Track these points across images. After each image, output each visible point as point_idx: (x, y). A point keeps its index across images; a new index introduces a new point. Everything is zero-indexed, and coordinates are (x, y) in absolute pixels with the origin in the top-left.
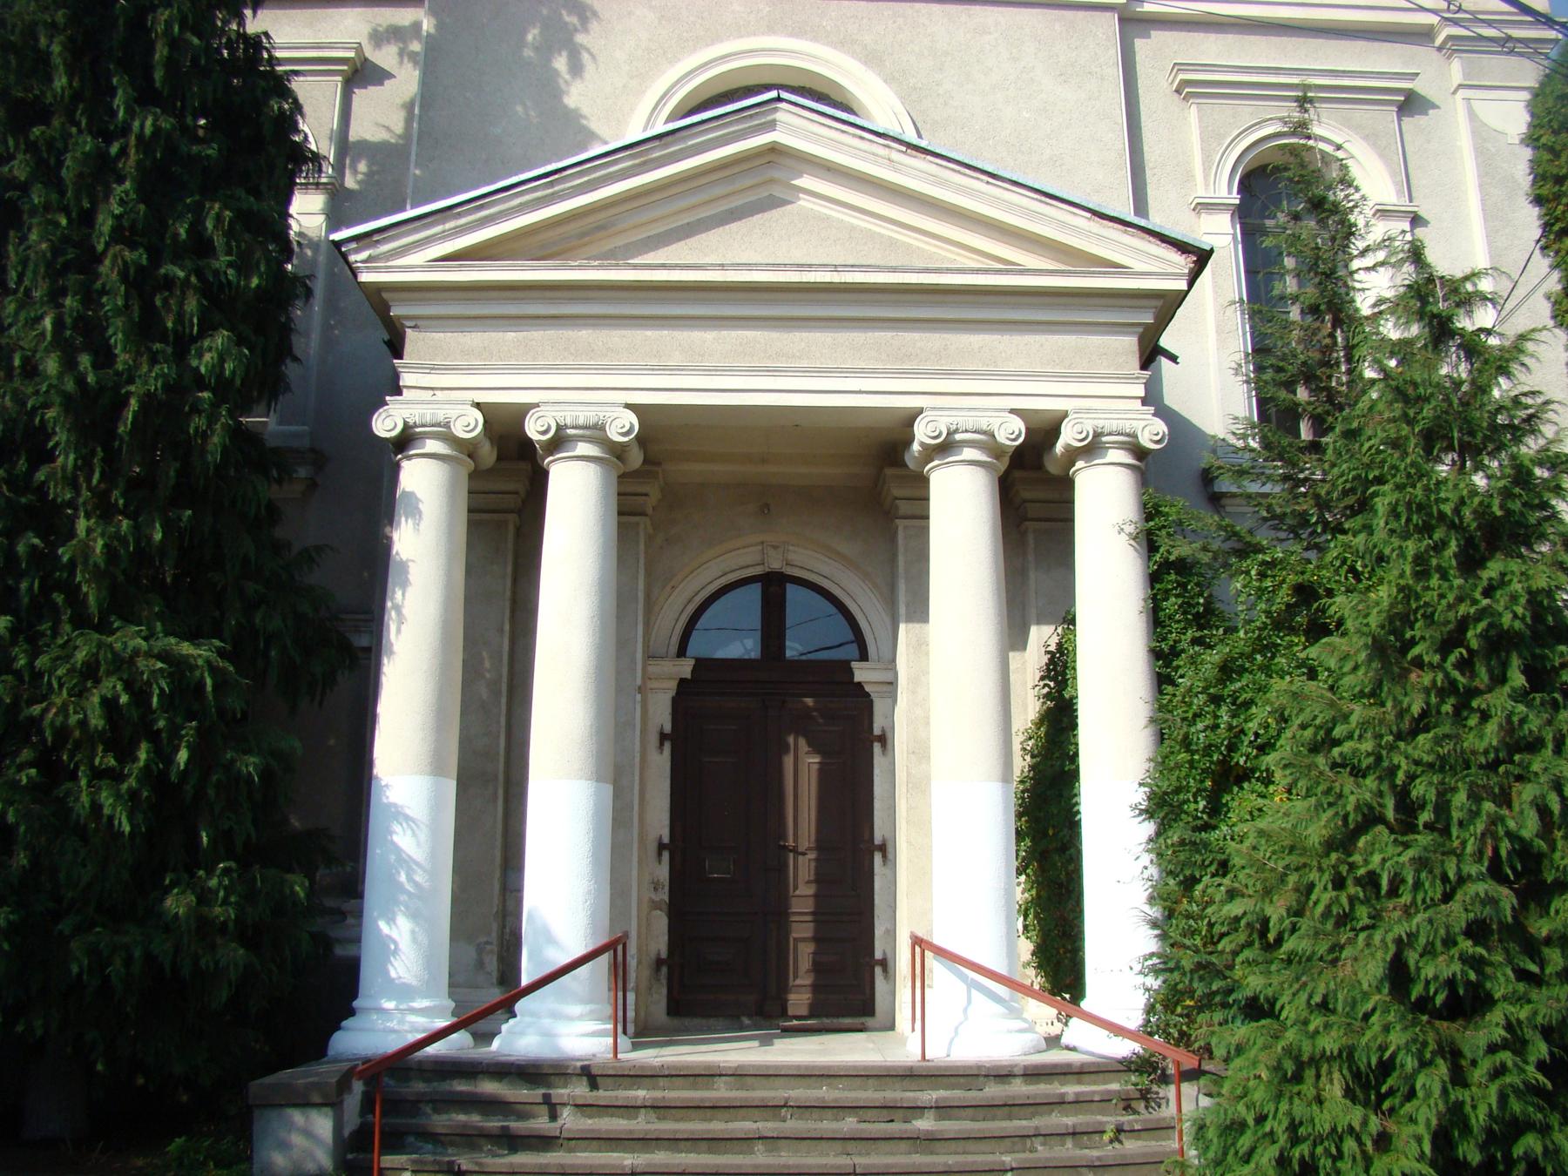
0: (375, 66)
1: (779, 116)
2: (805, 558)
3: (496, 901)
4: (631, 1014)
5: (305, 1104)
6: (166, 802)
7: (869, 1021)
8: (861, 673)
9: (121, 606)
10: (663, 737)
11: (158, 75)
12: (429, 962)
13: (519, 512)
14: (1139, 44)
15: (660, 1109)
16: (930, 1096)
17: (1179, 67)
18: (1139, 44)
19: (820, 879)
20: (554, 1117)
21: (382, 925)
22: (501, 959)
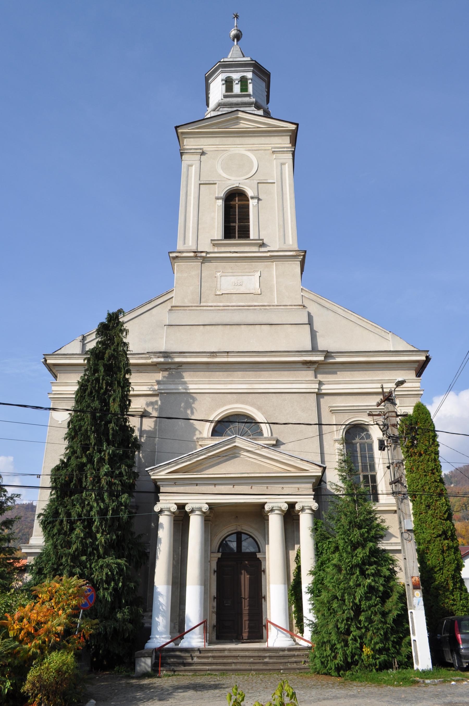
0: (148, 411)
1: (236, 440)
2: (246, 528)
3: (178, 612)
4: (208, 639)
5: (145, 657)
6: (117, 593)
7: (262, 640)
8: (259, 555)
9: (106, 553)
10: (215, 571)
11: (111, 437)
12: (165, 627)
13: (182, 520)
14: (322, 400)
15: (214, 657)
16: (267, 654)
17: (330, 407)
18: (322, 400)
19: (249, 605)
20: (192, 659)
21: (156, 619)
22: (179, 626)
